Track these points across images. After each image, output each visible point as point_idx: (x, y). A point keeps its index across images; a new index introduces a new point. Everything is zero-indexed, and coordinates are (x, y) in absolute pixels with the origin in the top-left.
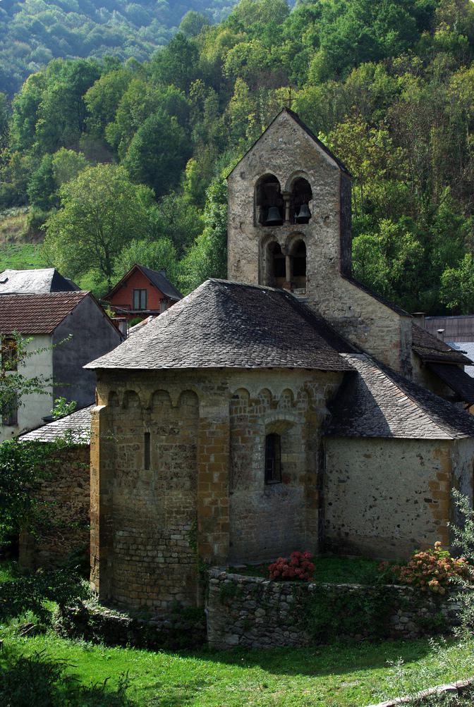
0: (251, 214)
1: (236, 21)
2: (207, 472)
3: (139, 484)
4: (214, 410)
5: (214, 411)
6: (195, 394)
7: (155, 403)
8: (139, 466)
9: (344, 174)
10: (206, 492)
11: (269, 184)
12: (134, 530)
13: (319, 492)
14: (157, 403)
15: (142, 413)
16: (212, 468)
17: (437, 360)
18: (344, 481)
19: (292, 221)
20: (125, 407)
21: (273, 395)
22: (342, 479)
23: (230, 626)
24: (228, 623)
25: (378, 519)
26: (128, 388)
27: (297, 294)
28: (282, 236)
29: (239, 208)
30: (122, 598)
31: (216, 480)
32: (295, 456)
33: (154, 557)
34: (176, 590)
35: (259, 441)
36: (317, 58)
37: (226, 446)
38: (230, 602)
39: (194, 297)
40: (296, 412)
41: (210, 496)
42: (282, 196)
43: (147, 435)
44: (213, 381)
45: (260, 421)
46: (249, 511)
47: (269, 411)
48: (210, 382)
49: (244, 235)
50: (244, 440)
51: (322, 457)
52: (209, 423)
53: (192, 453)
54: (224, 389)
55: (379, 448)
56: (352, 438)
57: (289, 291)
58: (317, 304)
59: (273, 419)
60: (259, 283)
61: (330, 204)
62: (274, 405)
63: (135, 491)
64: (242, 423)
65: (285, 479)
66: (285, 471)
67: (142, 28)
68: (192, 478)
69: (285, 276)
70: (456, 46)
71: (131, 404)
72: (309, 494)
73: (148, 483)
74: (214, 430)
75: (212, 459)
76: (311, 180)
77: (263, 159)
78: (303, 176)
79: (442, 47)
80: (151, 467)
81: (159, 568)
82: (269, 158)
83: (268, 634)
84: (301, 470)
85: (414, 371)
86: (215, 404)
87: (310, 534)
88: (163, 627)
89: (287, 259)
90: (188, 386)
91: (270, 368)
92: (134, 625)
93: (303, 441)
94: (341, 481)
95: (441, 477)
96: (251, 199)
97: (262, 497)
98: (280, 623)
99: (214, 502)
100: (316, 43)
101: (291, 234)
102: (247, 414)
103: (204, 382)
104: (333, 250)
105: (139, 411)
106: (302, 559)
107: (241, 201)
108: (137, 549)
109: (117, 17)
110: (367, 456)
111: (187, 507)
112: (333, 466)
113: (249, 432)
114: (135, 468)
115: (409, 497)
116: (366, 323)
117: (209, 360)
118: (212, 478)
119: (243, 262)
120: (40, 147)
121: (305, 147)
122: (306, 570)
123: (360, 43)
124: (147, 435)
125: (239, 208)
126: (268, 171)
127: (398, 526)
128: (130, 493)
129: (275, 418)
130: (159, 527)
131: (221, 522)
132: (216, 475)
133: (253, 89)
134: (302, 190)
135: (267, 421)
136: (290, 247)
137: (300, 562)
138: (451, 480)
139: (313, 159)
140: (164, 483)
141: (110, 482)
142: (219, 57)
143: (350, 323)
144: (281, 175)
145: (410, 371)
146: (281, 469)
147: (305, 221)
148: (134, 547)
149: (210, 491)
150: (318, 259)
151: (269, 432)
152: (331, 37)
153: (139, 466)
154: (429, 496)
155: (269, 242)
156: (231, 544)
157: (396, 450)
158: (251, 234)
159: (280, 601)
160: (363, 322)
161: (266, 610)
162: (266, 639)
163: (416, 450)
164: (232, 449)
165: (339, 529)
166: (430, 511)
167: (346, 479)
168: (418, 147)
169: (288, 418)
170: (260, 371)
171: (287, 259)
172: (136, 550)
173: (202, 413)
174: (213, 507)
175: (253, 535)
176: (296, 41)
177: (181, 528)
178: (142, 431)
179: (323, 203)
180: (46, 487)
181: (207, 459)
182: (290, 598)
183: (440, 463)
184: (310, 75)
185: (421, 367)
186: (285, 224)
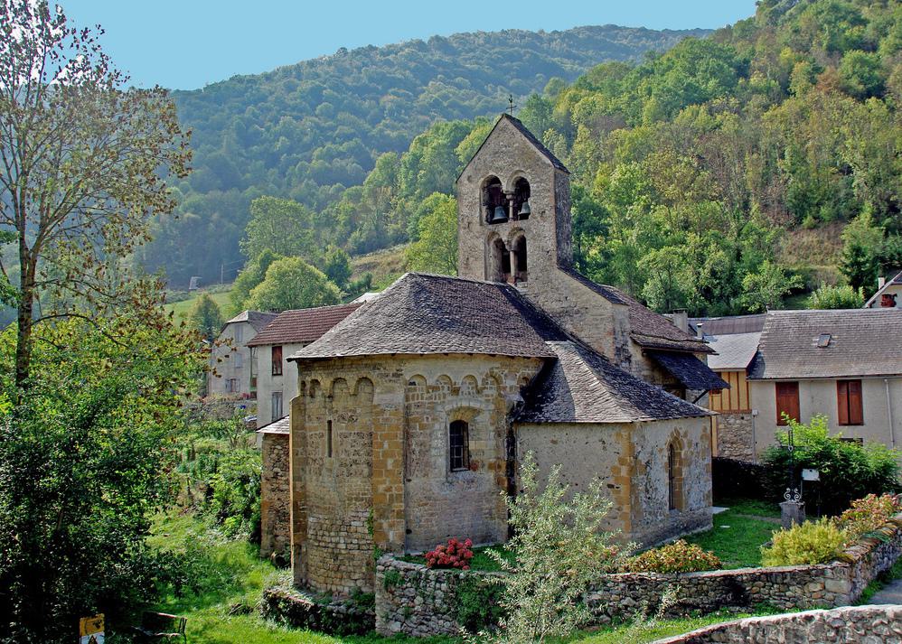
0: (478, 214)
1: (585, 81)
3: (324, 471)
4: (388, 397)
7: (336, 391)
8: (323, 454)
9: (559, 171)
10: (380, 479)
11: (494, 186)
12: (321, 516)
13: (509, 480)
14: (337, 391)
16: (386, 454)
17: (659, 347)
19: (516, 218)
20: (312, 396)
21: (453, 381)
23: (394, 614)
24: (392, 611)
27: (520, 288)
28: (504, 232)
30: (313, 583)
31: (390, 467)
32: (484, 444)
33: (337, 543)
34: (356, 577)
36: (650, 104)
37: (400, 433)
38: (393, 589)
40: (483, 399)
42: (505, 195)
43: (330, 422)
44: (387, 368)
45: (439, 408)
46: (429, 499)
47: (449, 398)
48: (385, 369)
50: (422, 427)
54: (399, 376)
56: (539, 423)
57: (513, 285)
59: (455, 406)
60: (486, 279)
62: (456, 391)
64: (419, 410)
65: (472, 467)
66: (473, 458)
67: (522, 97)
68: (369, 464)
69: (510, 271)
70: (769, 89)
72: (499, 482)
76: (529, 179)
78: (522, 175)
79: (757, 91)
80: (333, 455)
81: (341, 554)
83: (425, 622)
85: (633, 359)
86: (390, 391)
88: (338, 612)
89: (512, 255)
90: (364, 373)
91: (446, 354)
92: (315, 608)
93: (492, 428)
95: (622, 462)
98: (436, 612)
99: (389, 489)
100: (649, 92)
101: (513, 230)
103: (378, 369)
104: (549, 243)
106: (458, 547)
107: (469, 202)
109: (502, 90)
110: (554, 442)
111: (365, 494)
113: (427, 418)
117: (383, 347)
118: (386, 465)
120: (421, 193)
122: (462, 558)
123: (685, 90)
124: (330, 422)
126: (491, 173)
130: (341, 513)
131: (396, 509)
132: (390, 461)
133: (595, 135)
134: (522, 188)
135: (448, 407)
136: (513, 243)
137: (456, 550)
138: (633, 464)
141: (303, 469)
142: (568, 110)
145: (628, 359)
146: (469, 456)
148: (321, 533)
149: (384, 478)
151: (452, 419)
152: (660, 87)
153: (323, 454)
154: (611, 481)
155: (494, 239)
156: (408, 531)
157: (579, 435)
159: (435, 589)
161: (424, 598)
162: (424, 627)
163: (598, 434)
164: (407, 436)
169: (472, 404)
170: (437, 357)
171: (512, 255)
173: (376, 400)
174: (388, 494)
175: (434, 522)
176: (633, 93)
177: (360, 514)
179: (541, 199)
180: (281, 476)
181: (381, 445)
182: (444, 586)
183: (622, 447)
184: (644, 119)
185: (643, 355)
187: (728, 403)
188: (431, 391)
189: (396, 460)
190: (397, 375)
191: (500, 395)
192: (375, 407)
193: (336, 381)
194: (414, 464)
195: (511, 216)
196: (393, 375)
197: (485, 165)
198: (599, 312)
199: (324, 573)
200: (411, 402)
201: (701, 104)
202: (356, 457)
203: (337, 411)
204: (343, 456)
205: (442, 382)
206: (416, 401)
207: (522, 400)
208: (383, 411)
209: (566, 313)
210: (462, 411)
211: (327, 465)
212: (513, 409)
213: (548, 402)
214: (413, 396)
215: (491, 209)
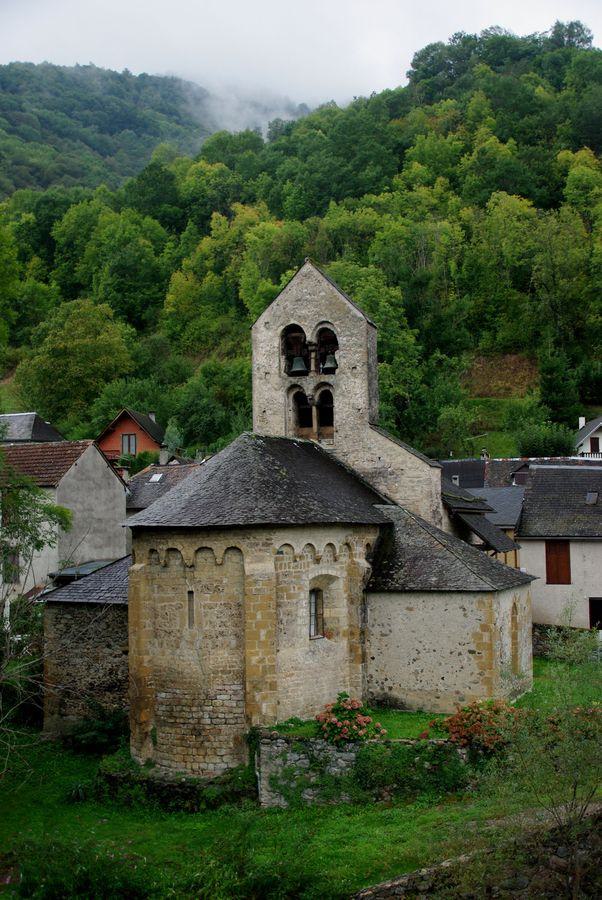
3: (183, 644)
5: (259, 567)
6: (239, 550)
11: (294, 335)
15: (184, 571)
18: (386, 635)
25: (422, 671)
26: (170, 545)
27: (324, 445)
31: (263, 638)
33: (199, 719)
34: (223, 752)
35: (304, 596)
37: (273, 604)
39: (231, 450)
40: (338, 567)
41: (257, 654)
45: (304, 577)
47: (312, 566)
49: (269, 386)
50: (289, 597)
51: (364, 611)
53: (240, 612)
55: (421, 601)
57: (316, 442)
58: (345, 455)
63: (178, 651)
69: (311, 425)
71: (172, 562)
72: (352, 649)
73: (192, 643)
75: (259, 617)
78: (329, 326)
80: (196, 626)
81: (204, 730)
84: (344, 626)
86: (260, 560)
87: (354, 689)
89: (314, 409)
93: (346, 595)
94: (383, 635)
96: (276, 350)
97: (307, 653)
99: (262, 661)
105: (182, 569)
108: (182, 711)
110: (410, 609)
111: (233, 666)
112: (375, 620)
114: (178, 628)
115: (453, 649)
116: (395, 474)
119: (268, 412)
126: (292, 322)
127: (443, 678)
128: (173, 654)
131: (269, 681)
132: (263, 632)
134: (328, 341)
135: (311, 576)
139: (339, 310)
140: (209, 642)
143: (379, 473)
147: (331, 371)
165: (383, 683)
166: (474, 662)
167: (388, 632)
168: (516, 314)
169: (330, 573)
171: (314, 409)
172: (180, 712)
173: (248, 568)
186: (311, 374)
187: (513, 560)
196: (263, 545)
198: (415, 474)
199: (183, 751)
200: (279, 571)
202: (223, 628)
208: (256, 582)
209: (379, 473)
211: (187, 637)
215: (290, 360)
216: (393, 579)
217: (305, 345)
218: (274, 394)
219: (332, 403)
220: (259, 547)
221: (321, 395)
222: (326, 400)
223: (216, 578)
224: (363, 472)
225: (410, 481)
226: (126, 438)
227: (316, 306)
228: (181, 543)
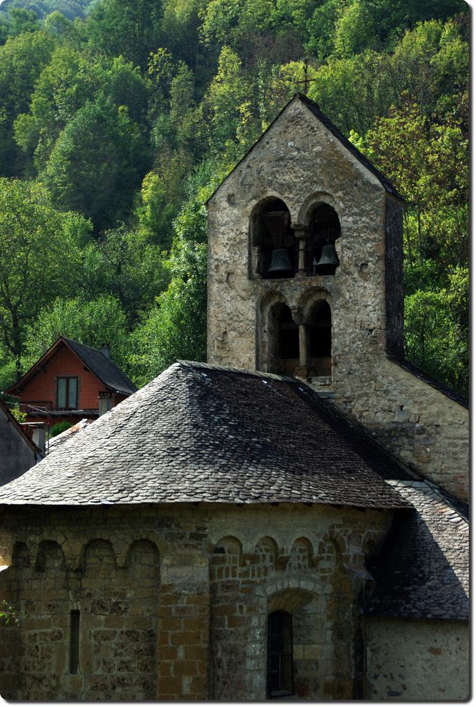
0: (245, 260)
2: (173, 676)
5: (184, 572)
7: (89, 561)
9: (391, 198)
14: (92, 560)
15: (67, 578)
19: (310, 270)
20: (40, 568)
22: (394, 689)
26: (46, 536)
28: (293, 294)
29: (225, 250)
35: (257, 625)
37: (204, 632)
39: (154, 389)
40: (316, 576)
44: (182, 524)
45: (259, 591)
47: (273, 574)
48: (178, 526)
49: (233, 293)
51: (360, 651)
52: (176, 593)
55: (454, 638)
57: (304, 381)
58: (349, 400)
60: (257, 369)
61: (369, 245)
64: (229, 594)
66: (300, 673)
74: (185, 605)
76: (339, 206)
77: (262, 173)
78: (327, 200)
80: (80, 669)
82: (273, 173)
86: (187, 562)
89: (302, 330)
91: (275, 504)
93: (329, 624)
96: (244, 237)
101: (308, 291)
102: (237, 578)
103: (168, 526)
104: (374, 316)
107: (229, 239)
112: (379, 667)
114: (53, 671)
117: (177, 491)
119: (232, 335)
121: (330, 155)
124: (75, 614)
125: (225, 250)
126: (271, 193)
129: (282, 585)
134: (324, 223)
135: (270, 590)
136: (306, 312)
144: (291, 199)
146: (294, 670)
150: (350, 330)
153: (60, 668)
155: (273, 303)
158: (244, 290)
160: (422, 431)
167: (400, 689)
169: (303, 585)
170: (258, 508)
171: (302, 330)
173: (166, 576)
178: (67, 608)
179: (358, 243)
181: (172, 654)
184: (338, 42)
186: (299, 276)
188: (248, 562)
189: (198, 679)
190: (198, 536)
191: (342, 569)
192: (165, 588)
193: (90, 545)
194: (220, 684)
195: (301, 265)
197: (260, 179)
200: (217, 580)
201: (445, 21)
202: (124, 673)
203: (89, 595)
204: (99, 672)
205: (263, 547)
206: (224, 579)
207: (371, 578)
210: (287, 596)
212: (361, 593)
213: (415, 583)
214: (220, 570)
216: (408, 601)
217: (290, 231)
218: (241, 306)
219: (330, 320)
220: (186, 540)
221: (313, 309)
222: (321, 316)
223: (117, 590)
224: (376, 430)
225: (450, 444)
226: (62, 383)
227: (307, 168)
228: (63, 532)
